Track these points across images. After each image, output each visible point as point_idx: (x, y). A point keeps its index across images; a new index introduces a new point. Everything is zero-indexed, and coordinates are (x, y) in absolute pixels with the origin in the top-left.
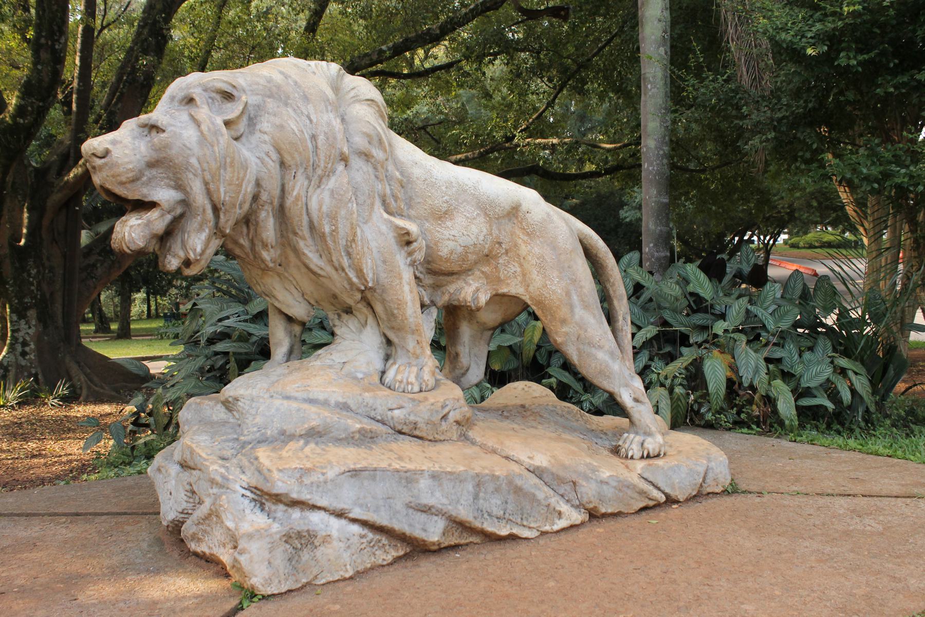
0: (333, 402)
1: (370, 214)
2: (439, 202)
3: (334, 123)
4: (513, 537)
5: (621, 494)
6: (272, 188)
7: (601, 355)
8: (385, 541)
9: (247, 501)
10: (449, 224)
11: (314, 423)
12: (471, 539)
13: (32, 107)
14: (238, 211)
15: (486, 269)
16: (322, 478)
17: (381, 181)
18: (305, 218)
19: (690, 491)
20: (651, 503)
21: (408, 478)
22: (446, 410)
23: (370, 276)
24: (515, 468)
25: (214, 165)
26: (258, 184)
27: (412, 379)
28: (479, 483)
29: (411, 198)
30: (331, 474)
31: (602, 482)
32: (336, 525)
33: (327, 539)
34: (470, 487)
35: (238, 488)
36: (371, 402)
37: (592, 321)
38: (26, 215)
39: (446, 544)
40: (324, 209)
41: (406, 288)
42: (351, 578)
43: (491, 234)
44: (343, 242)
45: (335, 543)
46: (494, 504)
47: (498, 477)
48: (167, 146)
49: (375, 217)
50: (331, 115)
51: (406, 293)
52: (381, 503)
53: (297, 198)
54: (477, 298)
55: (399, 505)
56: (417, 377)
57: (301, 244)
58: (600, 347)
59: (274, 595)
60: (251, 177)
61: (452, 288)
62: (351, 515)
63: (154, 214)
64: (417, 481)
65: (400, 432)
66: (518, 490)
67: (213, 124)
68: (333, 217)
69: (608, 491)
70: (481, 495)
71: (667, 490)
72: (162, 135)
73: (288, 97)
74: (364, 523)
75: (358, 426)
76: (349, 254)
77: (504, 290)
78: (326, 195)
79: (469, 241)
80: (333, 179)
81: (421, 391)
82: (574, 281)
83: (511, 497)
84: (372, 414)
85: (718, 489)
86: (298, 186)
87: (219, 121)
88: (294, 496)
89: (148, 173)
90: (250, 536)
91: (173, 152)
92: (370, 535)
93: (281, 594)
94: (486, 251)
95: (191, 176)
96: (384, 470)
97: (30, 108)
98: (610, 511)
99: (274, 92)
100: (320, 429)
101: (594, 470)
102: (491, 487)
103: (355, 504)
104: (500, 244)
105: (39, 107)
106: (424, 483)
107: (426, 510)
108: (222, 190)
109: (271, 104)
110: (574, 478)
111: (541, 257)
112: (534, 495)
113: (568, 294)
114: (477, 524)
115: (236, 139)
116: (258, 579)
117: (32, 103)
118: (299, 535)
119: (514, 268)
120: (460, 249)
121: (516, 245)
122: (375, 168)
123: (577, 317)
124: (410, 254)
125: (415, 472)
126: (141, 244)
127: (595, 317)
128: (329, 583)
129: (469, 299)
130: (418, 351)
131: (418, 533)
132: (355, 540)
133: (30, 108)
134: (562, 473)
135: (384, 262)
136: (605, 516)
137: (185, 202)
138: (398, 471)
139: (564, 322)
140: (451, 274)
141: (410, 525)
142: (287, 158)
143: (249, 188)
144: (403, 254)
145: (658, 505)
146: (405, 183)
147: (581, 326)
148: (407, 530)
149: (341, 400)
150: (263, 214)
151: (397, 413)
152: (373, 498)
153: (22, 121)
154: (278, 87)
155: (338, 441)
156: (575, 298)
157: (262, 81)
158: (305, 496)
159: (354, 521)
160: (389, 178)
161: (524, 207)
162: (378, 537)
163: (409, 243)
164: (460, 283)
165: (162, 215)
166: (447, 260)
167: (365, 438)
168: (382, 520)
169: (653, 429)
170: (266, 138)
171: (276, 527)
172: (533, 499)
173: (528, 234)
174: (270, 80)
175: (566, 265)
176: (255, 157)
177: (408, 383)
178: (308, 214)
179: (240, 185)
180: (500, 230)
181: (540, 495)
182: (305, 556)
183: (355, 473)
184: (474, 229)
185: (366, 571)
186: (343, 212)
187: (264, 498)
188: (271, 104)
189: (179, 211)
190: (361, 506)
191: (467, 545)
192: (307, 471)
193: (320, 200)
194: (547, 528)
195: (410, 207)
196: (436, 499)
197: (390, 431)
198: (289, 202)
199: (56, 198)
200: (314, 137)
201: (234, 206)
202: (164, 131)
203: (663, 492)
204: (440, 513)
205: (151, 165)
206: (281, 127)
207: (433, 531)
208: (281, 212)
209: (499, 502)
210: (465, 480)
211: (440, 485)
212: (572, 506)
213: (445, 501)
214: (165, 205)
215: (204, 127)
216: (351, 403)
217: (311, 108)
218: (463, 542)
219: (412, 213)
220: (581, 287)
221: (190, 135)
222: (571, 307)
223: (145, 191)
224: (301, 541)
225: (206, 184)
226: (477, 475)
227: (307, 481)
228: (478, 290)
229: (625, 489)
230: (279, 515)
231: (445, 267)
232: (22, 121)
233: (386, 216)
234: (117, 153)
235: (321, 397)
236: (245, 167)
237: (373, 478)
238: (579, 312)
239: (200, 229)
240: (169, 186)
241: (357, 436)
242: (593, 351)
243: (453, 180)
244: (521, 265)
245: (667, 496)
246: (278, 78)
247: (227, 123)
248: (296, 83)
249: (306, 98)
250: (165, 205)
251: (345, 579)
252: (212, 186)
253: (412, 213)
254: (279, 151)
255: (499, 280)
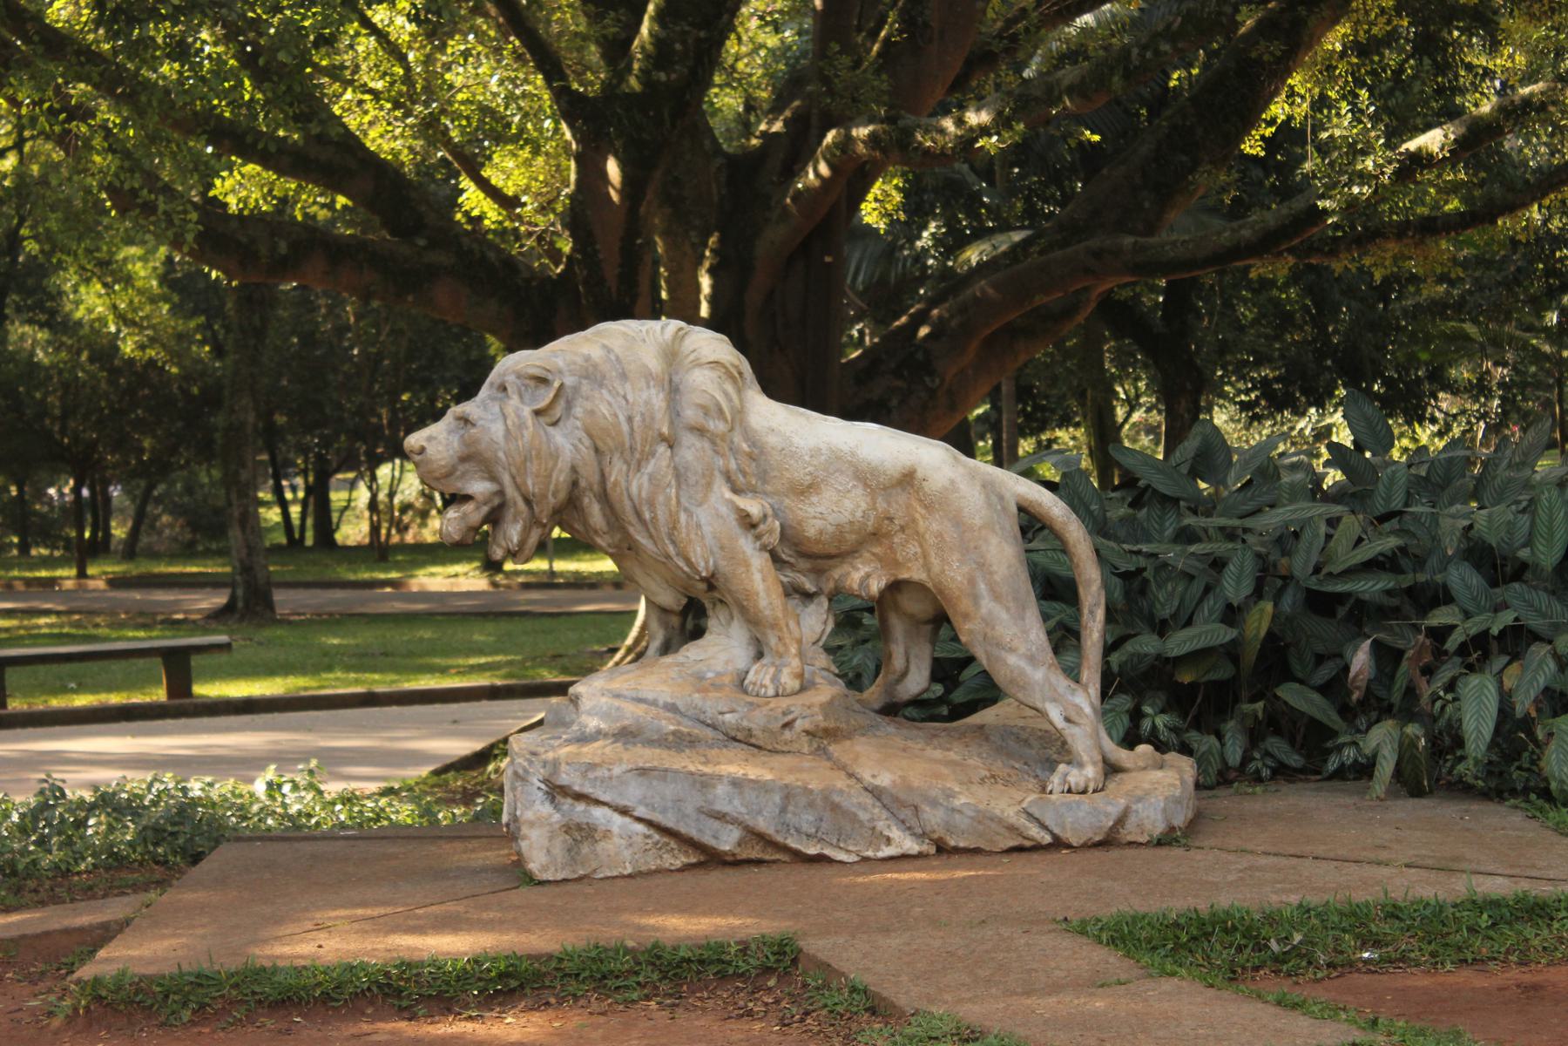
0: (661, 703)
1: (706, 496)
2: (800, 474)
3: (654, 401)
4: (821, 859)
5: (981, 827)
6: (589, 475)
7: (1012, 660)
8: (673, 844)
9: (540, 794)
10: (814, 499)
11: (626, 722)
12: (777, 856)
13: (684, 43)
14: (552, 500)
15: (877, 550)
16: (607, 774)
17: (723, 456)
18: (627, 503)
19: (1090, 835)
20: (1028, 844)
21: (704, 783)
22: (790, 717)
23: (701, 565)
24: (841, 782)
25: (518, 460)
26: (574, 469)
27: (767, 681)
28: (788, 794)
29: (765, 471)
30: (617, 771)
31: (953, 810)
32: (618, 820)
33: (607, 834)
34: (777, 799)
35: (535, 781)
36: (700, 704)
37: (1004, 615)
38: (706, 283)
39: (744, 856)
40: (644, 494)
41: (757, 577)
42: (630, 876)
43: (875, 509)
44: (664, 530)
45: (616, 840)
46: (806, 820)
47: (811, 791)
48: (476, 442)
49: (713, 498)
50: (653, 391)
51: (758, 579)
52: (669, 804)
53: (616, 484)
54: (868, 586)
55: (689, 809)
56: (775, 679)
57: (631, 530)
58: (1012, 650)
59: (549, 882)
60: (564, 464)
61: (836, 574)
62: (636, 814)
63: (469, 507)
64: (714, 787)
65: (735, 739)
66: (835, 807)
67: (519, 416)
68: (652, 504)
69: (961, 822)
70: (791, 808)
71: (1057, 831)
72: (473, 431)
73: (604, 377)
74: (650, 823)
75: (672, 728)
76: (673, 542)
77: (904, 575)
78: (645, 478)
79: (844, 517)
80: (653, 462)
81: (777, 695)
82: (982, 565)
83: (827, 815)
84: (702, 717)
85: (1143, 839)
86: (616, 471)
87: (527, 411)
88: (577, 788)
89: (461, 468)
90: (532, 824)
91: (483, 446)
92: (657, 837)
93: (556, 882)
94: (870, 529)
95: (208, 779)
96: (676, 772)
97: (678, 46)
98: (961, 845)
99: (592, 374)
100: (633, 729)
101: (950, 795)
102: (803, 801)
103: (640, 802)
104: (891, 519)
105: (698, 40)
106: (721, 790)
107: (721, 817)
108: (529, 482)
109: (586, 387)
110: (917, 801)
111: (940, 535)
112: (855, 815)
113: (972, 582)
114: (779, 839)
115: (555, 424)
116: (537, 863)
117: (685, 33)
118: (579, 827)
119: (913, 548)
120: (830, 529)
121: (914, 520)
122: (713, 443)
123: (984, 611)
124: (758, 537)
125: (712, 776)
126: (457, 537)
127: (1008, 610)
128: (607, 878)
129: (855, 586)
130: (781, 649)
131: (707, 839)
132: (639, 839)
133: (678, 46)
134: (902, 796)
135: (722, 548)
136: (957, 850)
137: (501, 493)
138: (692, 774)
139: (966, 616)
140: (830, 557)
141: (700, 831)
142: (600, 444)
143: (561, 477)
144: (750, 538)
145: (1037, 848)
146: (757, 453)
147: (989, 622)
148: (694, 833)
149: (669, 700)
150: (586, 501)
151: (728, 717)
152: (662, 798)
153: (663, 76)
154: (595, 366)
155: (650, 743)
156: (982, 587)
157: (579, 360)
158: (588, 790)
159: (639, 820)
160: (734, 450)
161: (919, 474)
162: (665, 840)
163: (754, 526)
164: (846, 568)
165: (478, 508)
166: (818, 542)
167: (681, 742)
168: (669, 821)
169: (1085, 758)
170: (578, 423)
171: (557, 817)
172: (854, 819)
173: (926, 507)
174: (588, 359)
175: (972, 545)
176: (566, 442)
177: (762, 686)
178: (631, 500)
179: (550, 476)
180: (889, 504)
181: (863, 816)
182: (585, 849)
183: (643, 772)
184: (848, 504)
185: (650, 873)
186: (661, 498)
187: (556, 791)
188: (586, 387)
189: (496, 501)
190: (647, 805)
191: (774, 862)
192: (592, 766)
193: (639, 485)
194: (870, 853)
195: (765, 482)
196: (735, 807)
197: (721, 737)
198: (609, 486)
199: (773, 238)
200: (630, 419)
201: (545, 497)
202: (474, 425)
203: (1051, 832)
204: (735, 821)
205: (464, 459)
206: (592, 413)
207: (727, 840)
208: (604, 497)
209: (811, 818)
210: (772, 790)
211: (741, 793)
212: (914, 834)
213: (743, 810)
214: (480, 498)
215: (509, 422)
216: (680, 704)
217: (628, 386)
218: (767, 857)
219: (769, 488)
220: (991, 573)
221: (497, 430)
222: (976, 599)
223: (459, 485)
224: (580, 834)
225: (513, 478)
226: (786, 786)
227: (591, 775)
228: (868, 576)
229: (988, 822)
230: (565, 807)
231: (816, 549)
232: (663, 76)
233: (728, 495)
234: (431, 450)
235: (650, 696)
236: (555, 456)
237: (664, 779)
238: (987, 605)
239: (515, 520)
240: (483, 478)
241: (671, 738)
242: (1003, 654)
243: (822, 446)
244: (921, 546)
245: (1055, 837)
246: (596, 353)
247: (537, 413)
248: (618, 358)
249: (624, 376)
250: (480, 498)
251: (624, 877)
252: (519, 480)
253: (769, 488)
254: (590, 436)
255: (897, 564)
